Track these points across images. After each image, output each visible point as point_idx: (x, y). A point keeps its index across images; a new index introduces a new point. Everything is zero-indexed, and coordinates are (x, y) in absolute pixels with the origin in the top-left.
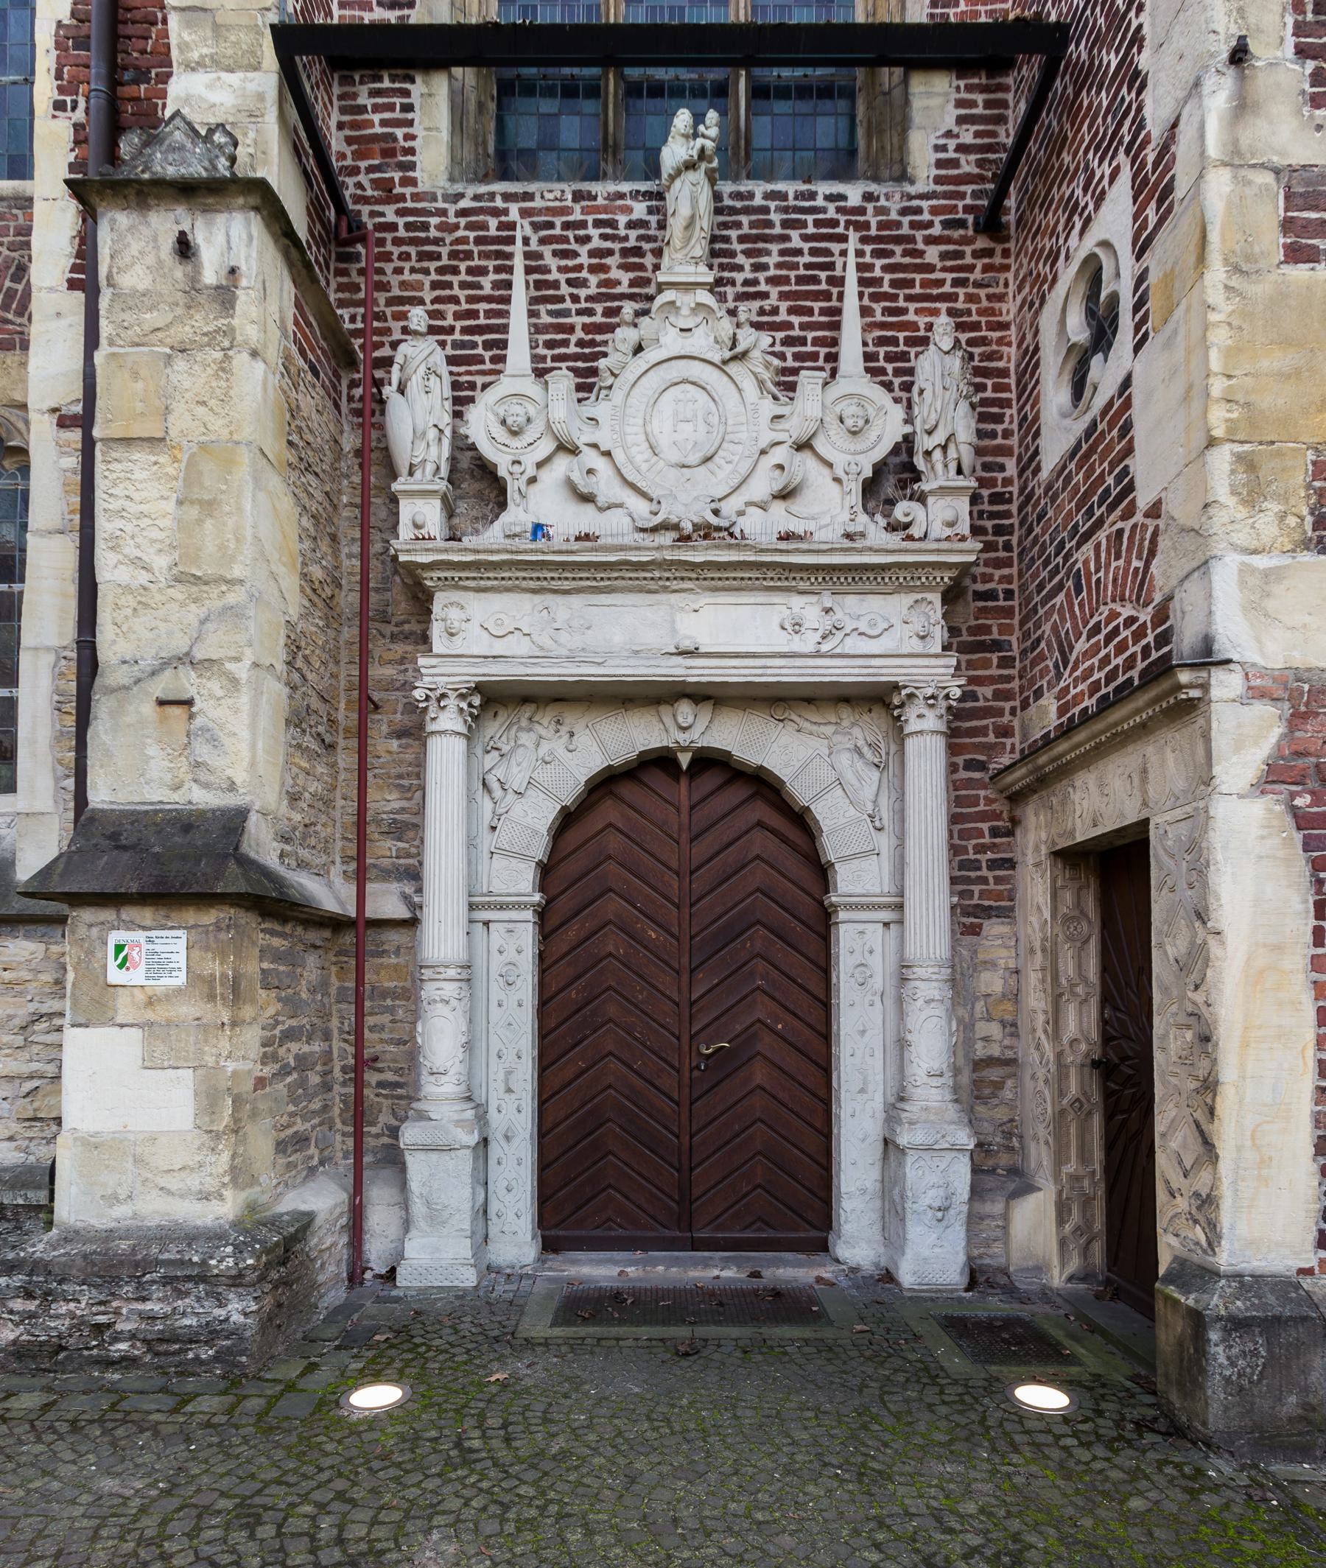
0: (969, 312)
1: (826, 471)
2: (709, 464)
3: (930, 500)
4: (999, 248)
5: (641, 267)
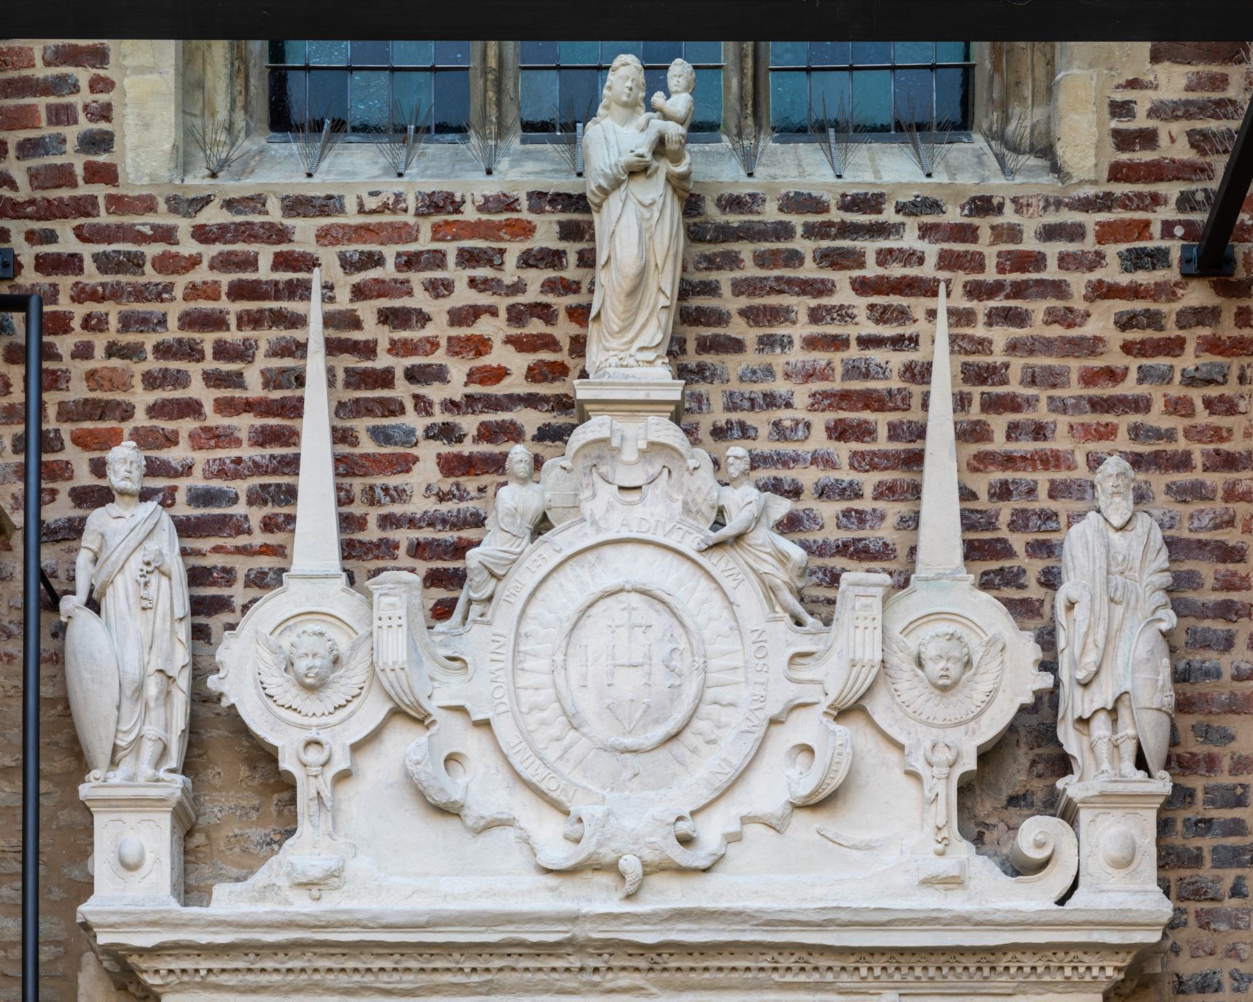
0: (1170, 435)
1: (892, 756)
2: (675, 747)
3: (1084, 816)
4: (1230, 308)
5: (550, 343)
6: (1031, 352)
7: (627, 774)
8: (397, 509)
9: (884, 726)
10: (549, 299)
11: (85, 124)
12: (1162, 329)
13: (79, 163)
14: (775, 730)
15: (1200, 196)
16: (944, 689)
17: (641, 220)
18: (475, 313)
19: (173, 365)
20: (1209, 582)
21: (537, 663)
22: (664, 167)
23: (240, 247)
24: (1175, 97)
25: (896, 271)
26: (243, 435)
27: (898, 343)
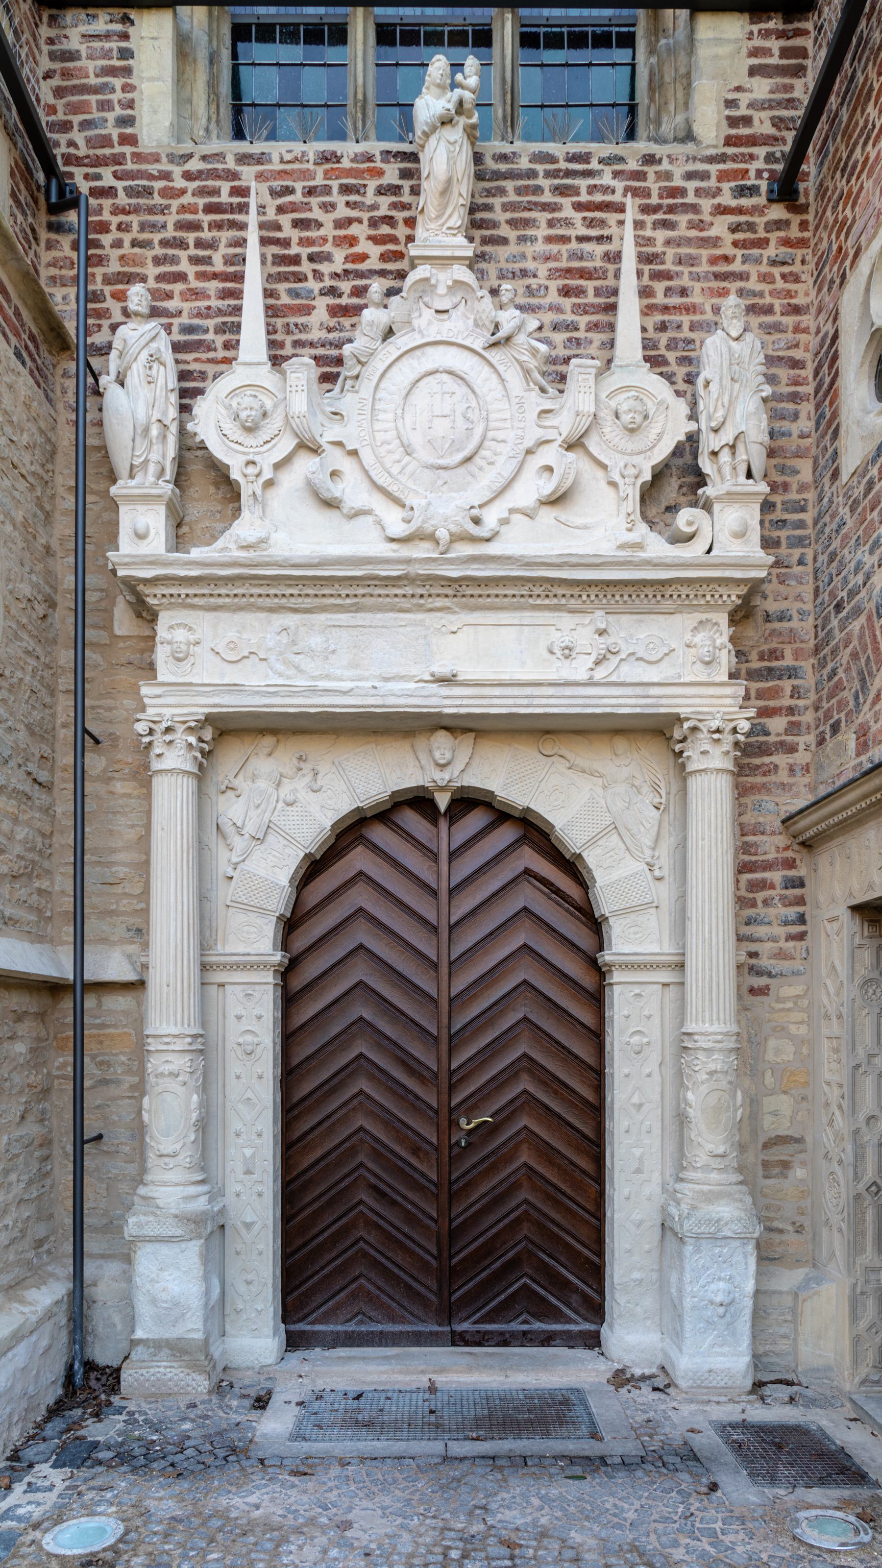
0: (761, 294)
1: (600, 473)
2: (470, 466)
3: (717, 507)
4: (796, 220)
5: (394, 240)
6: (679, 245)
7: (440, 482)
8: (303, 337)
9: (595, 454)
10: (393, 213)
11: (118, 111)
12: (755, 232)
13: (115, 134)
14: (529, 457)
15: (778, 155)
16: (632, 431)
17: (449, 152)
18: (349, 221)
19: (171, 252)
20: (784, 380)
21: (386, 417)
22: (462, 121)
23: (210, 183)
24: (763, 97)
25: (598, 198)
26: (212, 293)
27: (600, 239)
